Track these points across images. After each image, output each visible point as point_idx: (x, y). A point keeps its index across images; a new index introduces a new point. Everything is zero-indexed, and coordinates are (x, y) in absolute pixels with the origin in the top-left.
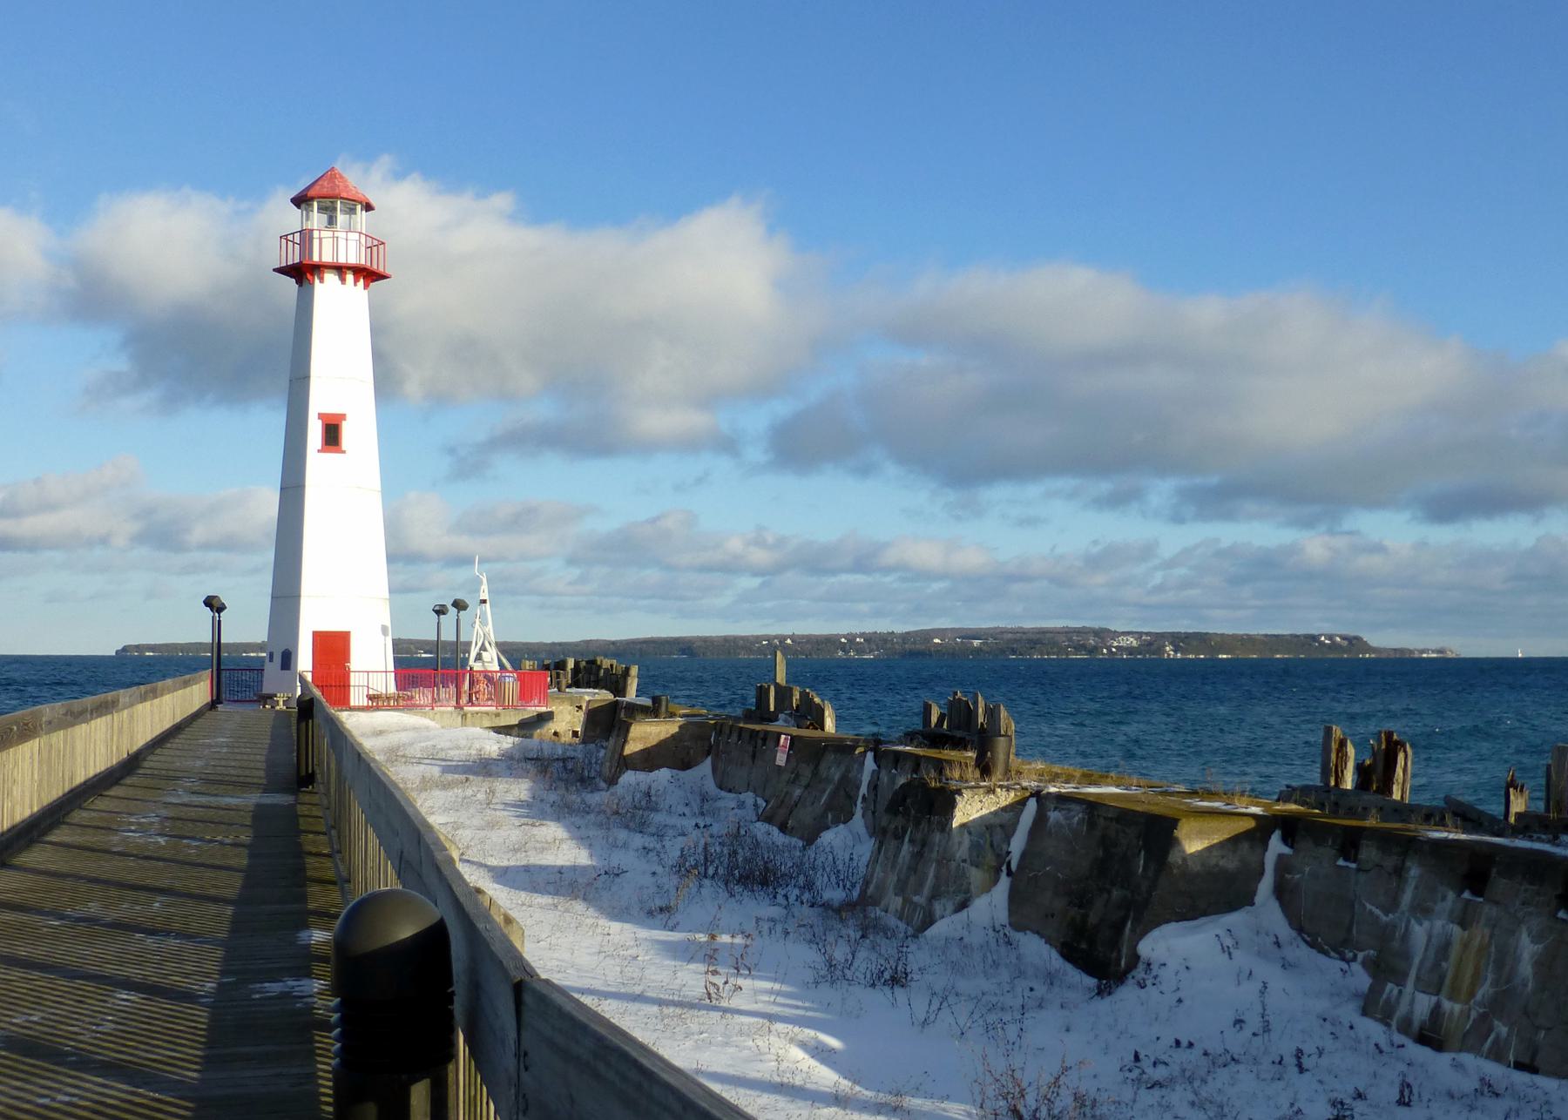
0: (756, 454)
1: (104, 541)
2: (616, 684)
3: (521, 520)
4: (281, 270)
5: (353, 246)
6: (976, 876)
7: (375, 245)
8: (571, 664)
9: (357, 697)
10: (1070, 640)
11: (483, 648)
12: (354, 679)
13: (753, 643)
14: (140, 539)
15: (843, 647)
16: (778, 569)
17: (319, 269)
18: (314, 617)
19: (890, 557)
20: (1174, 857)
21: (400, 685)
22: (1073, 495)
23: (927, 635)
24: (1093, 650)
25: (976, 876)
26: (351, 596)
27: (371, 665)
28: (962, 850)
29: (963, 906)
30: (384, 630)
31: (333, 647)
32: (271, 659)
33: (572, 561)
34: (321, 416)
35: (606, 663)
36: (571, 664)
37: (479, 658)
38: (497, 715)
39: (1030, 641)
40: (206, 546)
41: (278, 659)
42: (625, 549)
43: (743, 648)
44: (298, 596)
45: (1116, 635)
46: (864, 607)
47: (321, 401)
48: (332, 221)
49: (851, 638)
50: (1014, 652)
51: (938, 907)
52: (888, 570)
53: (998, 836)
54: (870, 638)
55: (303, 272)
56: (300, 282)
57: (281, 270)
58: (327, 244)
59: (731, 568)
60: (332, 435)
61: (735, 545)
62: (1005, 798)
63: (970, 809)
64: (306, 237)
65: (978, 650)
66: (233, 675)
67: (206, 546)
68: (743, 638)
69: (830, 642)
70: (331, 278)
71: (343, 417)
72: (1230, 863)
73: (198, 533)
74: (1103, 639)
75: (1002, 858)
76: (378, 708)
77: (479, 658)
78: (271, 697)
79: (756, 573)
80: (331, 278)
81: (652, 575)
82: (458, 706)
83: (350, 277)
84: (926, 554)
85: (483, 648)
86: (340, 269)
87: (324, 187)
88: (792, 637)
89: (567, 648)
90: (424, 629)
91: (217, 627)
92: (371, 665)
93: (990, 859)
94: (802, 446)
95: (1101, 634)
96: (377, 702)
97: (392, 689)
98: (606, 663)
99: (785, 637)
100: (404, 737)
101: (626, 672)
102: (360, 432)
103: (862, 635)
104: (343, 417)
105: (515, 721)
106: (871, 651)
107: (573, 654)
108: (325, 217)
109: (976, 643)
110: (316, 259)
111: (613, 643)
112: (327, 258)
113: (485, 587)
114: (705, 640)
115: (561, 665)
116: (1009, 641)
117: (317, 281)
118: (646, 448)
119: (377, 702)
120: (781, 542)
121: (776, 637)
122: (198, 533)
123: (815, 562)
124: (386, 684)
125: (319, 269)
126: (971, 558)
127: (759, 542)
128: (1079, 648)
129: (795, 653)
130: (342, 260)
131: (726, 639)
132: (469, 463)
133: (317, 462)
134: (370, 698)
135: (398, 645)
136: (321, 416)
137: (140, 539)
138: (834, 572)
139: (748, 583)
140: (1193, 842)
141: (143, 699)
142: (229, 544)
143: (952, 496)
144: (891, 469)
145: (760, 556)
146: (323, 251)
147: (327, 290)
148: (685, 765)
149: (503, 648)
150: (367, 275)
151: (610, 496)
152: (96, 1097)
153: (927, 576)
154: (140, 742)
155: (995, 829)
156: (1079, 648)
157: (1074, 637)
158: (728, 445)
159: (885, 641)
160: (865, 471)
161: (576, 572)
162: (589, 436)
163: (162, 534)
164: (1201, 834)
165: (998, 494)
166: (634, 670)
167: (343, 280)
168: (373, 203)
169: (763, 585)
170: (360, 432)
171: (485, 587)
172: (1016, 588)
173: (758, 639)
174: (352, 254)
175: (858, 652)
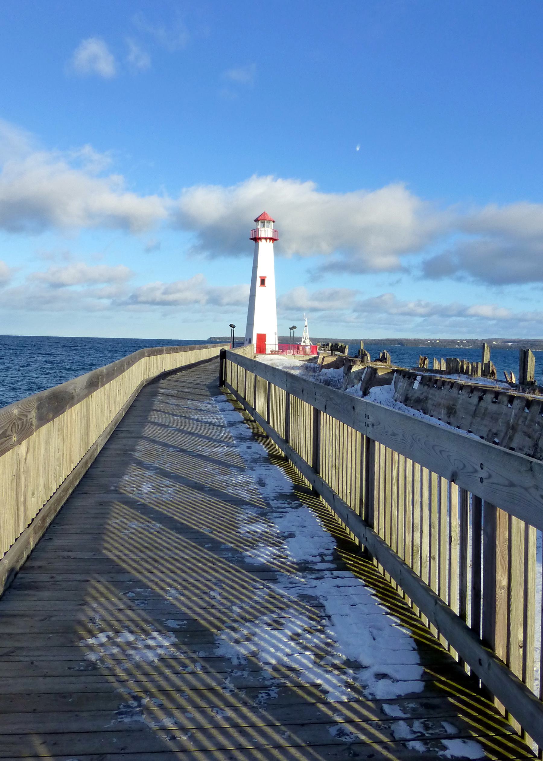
0: (418, 273)
1: (197, 302)
2: (342, 350)
3: (333, 296)
4: (251, 239)
5: (269, 232)
6: (356, 381)
7: (275, 231)
8: (330, 344)
9: (268, 351)
11: (306, 339)
12: (267, 346)
13: (424, 342)
14: (209, 302)
15: (458, 344)
16: (429, 315)
17: (260, 239)
18: (257, 330)
19: (472, 311)
20: (377, 375)
21: (279, 349)
25: (356, 381)
26: (268, 323)
27: (272, 343)
28: (353, 376)
29: (353, 386)
30: (275, 333)
33: (355, 311)
34: (260, 277)
35: (340, 345)
36: (330, 344)
37: (304, 342)
40: (228, 304)
41: (248, 341)
42: (370, 307)
43: (421, 343)
46: (464, 330)
48: (264, 226)
49: (462, 341)
51: (348, 386)
52: (472, 316)
53: (360, 374)
54: (468, 341)
55: (256, 239)
56: (256, 242)
57: (251, 239)
58: (263, 232)
59: (411, 314)
60: (263, 282)
61: (411, 305)
62: (362, 367)
63: (355, 369)
64: (257, 231)
65: (510, 347)
67: (228, 304)
68: (421, 340)
69: (454, 342)
70: (263, 240)
72: (387, 377)
73: (226, 300)
75: (361, 378)
76: (273, 354)
77: (304, 342)
79: (422, 316)
80: (263, 240)
81: (384, 316)
82: (293, 354)
83: (268, 240)
84: (486, 310)
85: (306, 339)
86: (266, 239)
87: (262, 217)
89: (331, 340)
90: (287, 334)
92: (272, 343)
93: (358, 378)
94: (435, 270)
96: (272, 352)
97: (277, 349)
98: (340, 345)
99: (463, 340)
100: (277, 361)
101: (345, 347)
103: (465, 340)
106: (469, 346)
108: (263, 224)
109: (510, 344)
110: (260, 236)
111: (374, 340)
112: (262, 236)
113: (306, 322)
114: (407, 340)
115: (328, 345)
118: (376, 271)
119: (272, 352)
120: (427, 305)
121: (433, 340)
122: (226, 300)
123: (444, 313)
124: (276, 348)
125: (260, 239)
126: (503, 313)
130: (266, 236)
131: (415, 340)
132: (315, 276)
134: (271, 351)
135: (280, 339)
136: (260, 277)
137: (209, 302)
138: (449, 316)
139: (419, 320)
140: (380, 373)
141: (213, 347)
142: (237, 303)
143: (494, 289)
144: (471, 279)
145: (421, 310)
146: (262, 234)
147: (262, 244)
148: (338, 368)
149: (311, 339)
150: (273, 240)
151: (366, 287)
152: (178, 499)
154: (212, 356)
155: (360, 372)
158: (406, 270)
160: (460, 279)
161: (356, 314)
162: (359, 268)
163: (215, 300)
164: (382, 372)
165: (511, 289)
166: (347, 347)
168: (275, 220)
169: (424, 320)
171: (306, 322)
172: (522, 324)
173: (427, 340)
174: (270, 234)
175: (464, 346)
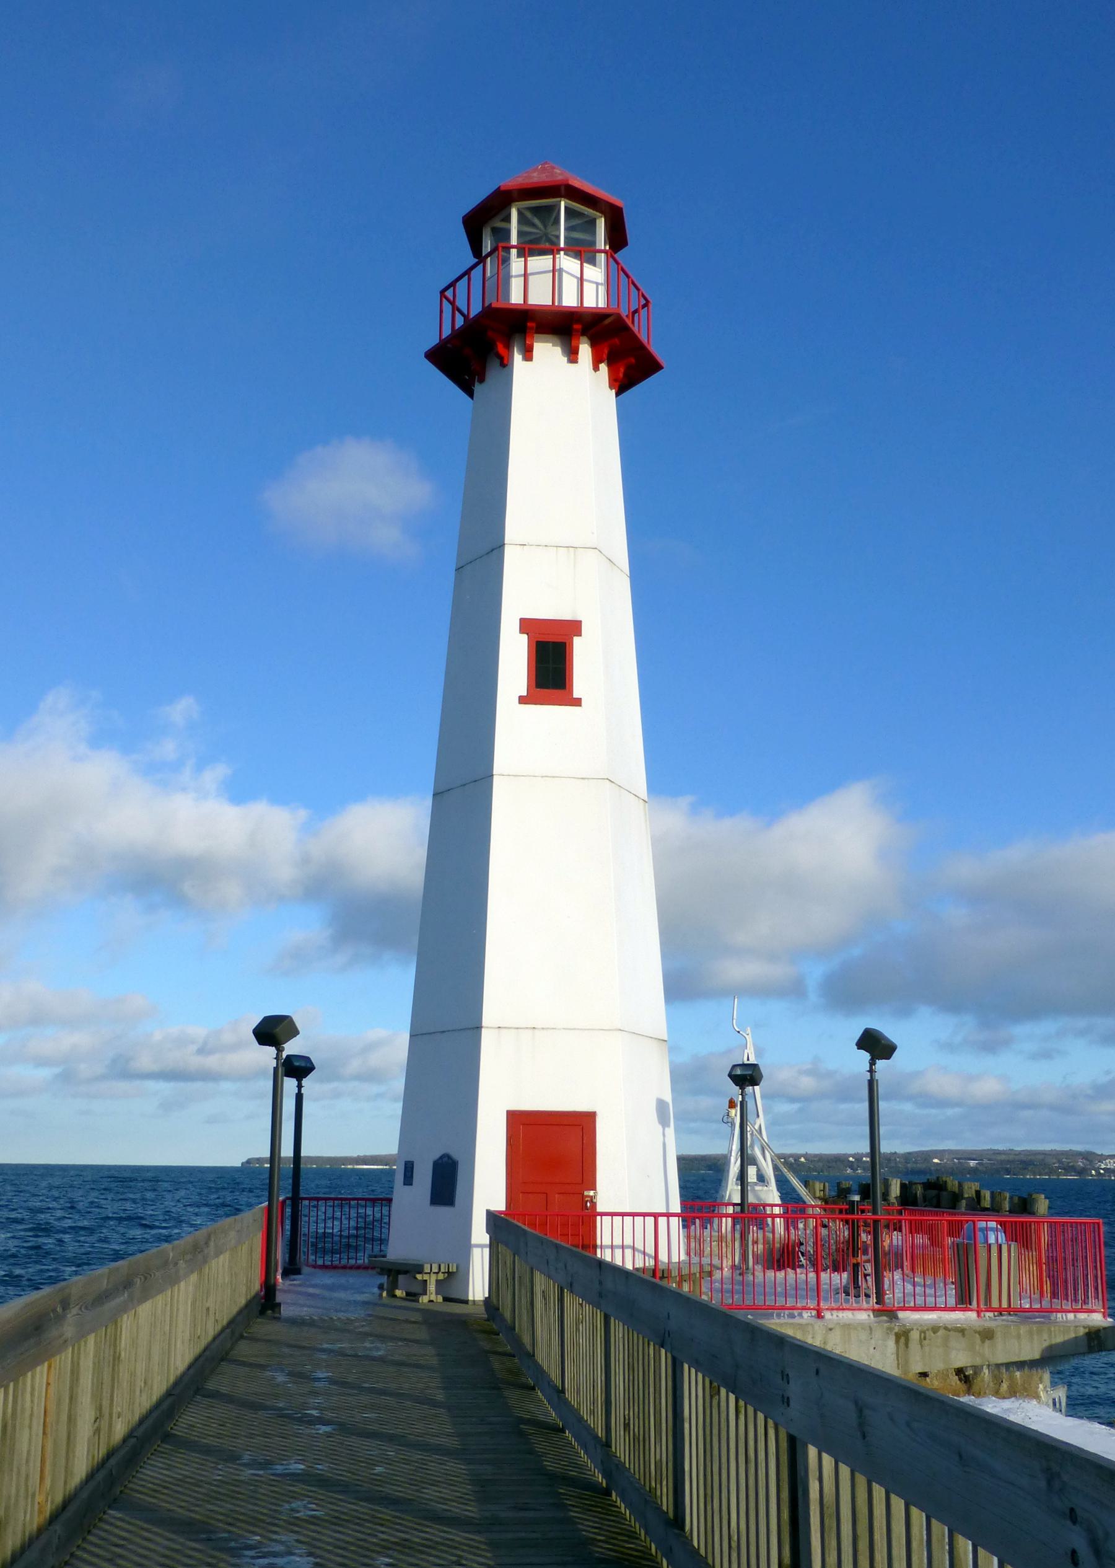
0: (813, 997)
10: (1060, 1162)
15: (851, 1165)
18: (510, 1081)
22: (1081, 1033)
23: (927, 1156)
24: (1082, 1172)
31: (554, 1147)
32: (408, 1180)
34: (526, 625)
38: (987, 1335)
39: (1022, 1162)
44: (476, 1028)
45: (1102, 1158)
47: (528, 591)
50: (1008, 1172)
60: (552, 666)
66: (307, 1213)
71: (574, 627)
74: (1091, 1162)
78: (411, 1270)
80: (547, 351)
88: (805, 1156)
91: (300, 1086)
95: (1089, 1156)
102: (606, 662)
104: (574, 627)
105: (1031, 1350)
107: (896, 1173)
109: (972, 1163)
110: (516, 298)
116: (1002, 1162)
117: (518, 357)
121: (791, 1156)
126: (988, 1088)
127: (813, 1072)
128: (1069, 1169)
129: (810, 1170)
133: (520, 729)
136: (526, 625)
145: (807, 1083)
153: (942, 1103)
156: (1069, 1169)
157: (1065, 1161)
158: (794, 990)
159: (889, 1160)
167: (572, 355)
170: (606, 662)
172: (1028, 1113)
